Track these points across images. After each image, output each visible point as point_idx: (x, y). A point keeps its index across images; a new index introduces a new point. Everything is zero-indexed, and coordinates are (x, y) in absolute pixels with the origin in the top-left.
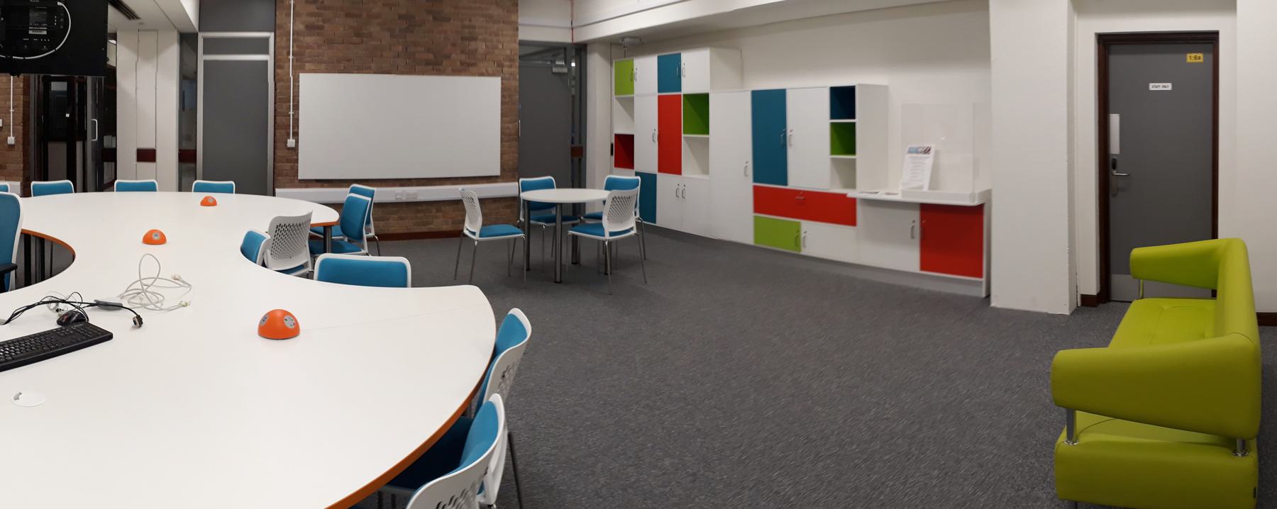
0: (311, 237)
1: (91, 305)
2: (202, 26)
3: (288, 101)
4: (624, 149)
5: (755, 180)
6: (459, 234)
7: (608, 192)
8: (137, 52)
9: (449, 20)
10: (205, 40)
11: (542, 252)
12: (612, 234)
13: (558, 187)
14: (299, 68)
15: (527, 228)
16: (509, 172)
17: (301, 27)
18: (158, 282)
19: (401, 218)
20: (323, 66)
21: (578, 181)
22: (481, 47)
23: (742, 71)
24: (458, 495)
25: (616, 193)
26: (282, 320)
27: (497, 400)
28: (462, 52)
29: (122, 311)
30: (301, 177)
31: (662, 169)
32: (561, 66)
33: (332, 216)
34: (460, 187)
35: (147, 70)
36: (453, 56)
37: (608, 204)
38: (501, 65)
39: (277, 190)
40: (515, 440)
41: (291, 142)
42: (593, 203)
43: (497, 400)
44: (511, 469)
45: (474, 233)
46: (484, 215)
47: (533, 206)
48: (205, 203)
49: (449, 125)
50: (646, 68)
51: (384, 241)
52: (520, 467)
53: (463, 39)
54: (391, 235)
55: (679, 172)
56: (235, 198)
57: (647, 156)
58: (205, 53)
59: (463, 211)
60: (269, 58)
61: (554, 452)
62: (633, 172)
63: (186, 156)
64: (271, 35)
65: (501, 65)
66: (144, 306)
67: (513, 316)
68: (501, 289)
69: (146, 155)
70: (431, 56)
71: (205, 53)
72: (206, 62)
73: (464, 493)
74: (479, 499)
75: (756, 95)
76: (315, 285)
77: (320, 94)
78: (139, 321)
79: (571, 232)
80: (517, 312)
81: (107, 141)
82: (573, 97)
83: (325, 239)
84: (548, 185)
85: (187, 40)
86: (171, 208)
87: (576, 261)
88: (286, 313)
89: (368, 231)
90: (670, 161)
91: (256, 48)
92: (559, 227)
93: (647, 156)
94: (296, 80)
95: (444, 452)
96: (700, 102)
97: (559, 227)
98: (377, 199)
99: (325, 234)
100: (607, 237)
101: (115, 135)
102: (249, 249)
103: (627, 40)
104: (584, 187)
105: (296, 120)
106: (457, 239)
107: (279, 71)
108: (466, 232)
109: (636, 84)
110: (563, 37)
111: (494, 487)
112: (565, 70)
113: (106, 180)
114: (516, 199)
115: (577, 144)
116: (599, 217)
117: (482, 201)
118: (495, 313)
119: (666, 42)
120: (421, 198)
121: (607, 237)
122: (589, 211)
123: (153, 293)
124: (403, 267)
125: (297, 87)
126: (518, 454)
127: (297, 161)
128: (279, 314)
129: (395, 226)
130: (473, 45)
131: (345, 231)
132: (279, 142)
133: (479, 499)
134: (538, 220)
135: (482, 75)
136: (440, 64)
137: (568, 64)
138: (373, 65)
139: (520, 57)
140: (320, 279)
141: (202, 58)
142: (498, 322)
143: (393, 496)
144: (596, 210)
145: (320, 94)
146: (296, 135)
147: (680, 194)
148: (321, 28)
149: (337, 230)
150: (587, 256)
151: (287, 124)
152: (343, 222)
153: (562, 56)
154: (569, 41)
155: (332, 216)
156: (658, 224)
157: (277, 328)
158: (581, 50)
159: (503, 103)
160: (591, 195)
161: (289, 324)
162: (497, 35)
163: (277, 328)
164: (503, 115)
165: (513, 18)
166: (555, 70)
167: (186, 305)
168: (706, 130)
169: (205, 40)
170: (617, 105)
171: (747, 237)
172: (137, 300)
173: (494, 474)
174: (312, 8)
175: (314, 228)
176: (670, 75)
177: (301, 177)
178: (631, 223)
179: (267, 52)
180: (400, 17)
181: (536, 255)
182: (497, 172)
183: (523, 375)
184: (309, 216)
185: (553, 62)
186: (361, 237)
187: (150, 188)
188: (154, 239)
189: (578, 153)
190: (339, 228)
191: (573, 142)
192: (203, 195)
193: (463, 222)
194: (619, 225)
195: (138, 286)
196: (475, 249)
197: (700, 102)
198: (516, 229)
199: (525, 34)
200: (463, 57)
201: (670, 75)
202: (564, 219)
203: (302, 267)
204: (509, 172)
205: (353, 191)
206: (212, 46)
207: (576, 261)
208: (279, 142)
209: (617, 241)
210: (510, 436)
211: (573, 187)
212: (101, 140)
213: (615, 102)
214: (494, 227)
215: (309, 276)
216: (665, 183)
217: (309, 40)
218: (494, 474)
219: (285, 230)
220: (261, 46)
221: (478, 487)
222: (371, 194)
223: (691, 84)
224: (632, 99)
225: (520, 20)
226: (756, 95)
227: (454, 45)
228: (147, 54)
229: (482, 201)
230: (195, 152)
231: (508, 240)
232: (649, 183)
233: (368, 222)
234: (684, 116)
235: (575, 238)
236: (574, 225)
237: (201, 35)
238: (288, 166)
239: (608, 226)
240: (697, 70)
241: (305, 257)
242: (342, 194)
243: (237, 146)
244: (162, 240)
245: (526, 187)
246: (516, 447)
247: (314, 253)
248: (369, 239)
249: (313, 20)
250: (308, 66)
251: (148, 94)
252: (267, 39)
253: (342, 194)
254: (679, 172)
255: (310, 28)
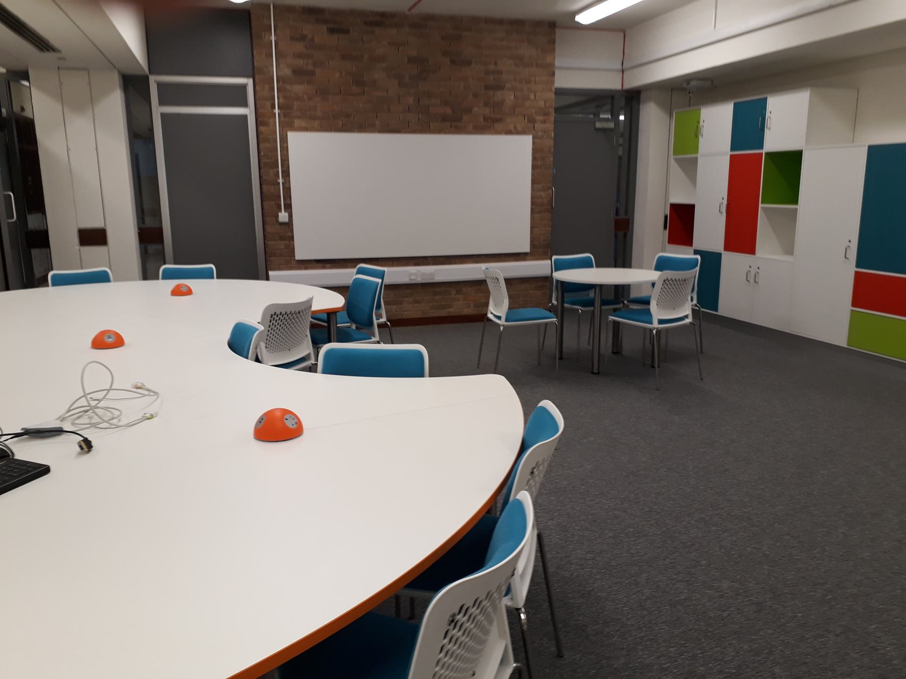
0: (313, 326)
1: (17, 435)
2: (154, 67)
3: (275, 165)
4: (681, 222)
5: (858, 266)
6: (482, 318)
7: (658, 273)
8: (61, 98)
9: (469, 63)
10: (160, 86)
11: (577, 338)
12: (661, 322)
13: (597, 266)
14: (288, 125)
15: (561, 313)
16: (539, 249)
17: (287, 72)
18: (112, 394)
19: (416, 302)
20: (316, 123)
21: (622, 259)
22: (509, 98)
23: (855, 120)
24: (483, 597)
25: (669, 274)
26: (282, 419)
27: (525, 498)
28: (486, 105)
29: (64, 437)
30: (299, 256)
31: (730, 246)
32: (607, 120)
33: (336, 301)
34: (483, 266)
35: (80, 125)
36: (475, 109)
37: (658, 286)
38: (532, 120)
39: (271, 273)
40: (546, 541)
41: (283, 216)
42: (639, 285)
43: (525, 498)
44: (541, 564)
45: (499, 318)
46: (510, 297)
47: (567, 288)
48: (177, 292)
49: (473, 193)
50: (717, 121)
51: (396, 327)
52: (551, 570)
53: (487, 88)
54: (404, 320)
55: (751, 250)
56: (216, 284)
57: (710, 230)
58: (162, 103)
59: (487, 293)
60: (248, 111)
61: (589, 556)
62: (691, 249)
63: (149, 236)
64: (249, 82)
65: (532, 120)
66: (94, 425)
67: (544, 409)
68: (528, 379)
69: (93, 237)
70: (448, 111)
71: (245, 117)
72: (164, 116)
73: (489, 595)
74: (506, 601)
75: (876, 154)
76: (319, 379)
77: (311, 155)
78: (87, 445)
79: (611, 318)
80: (547, 404)
81: (33, 222)
82: (620, 158)
83: (329, 327)
84: (586, 264)
85: (134, 86)
86: (130, 302)
87: (617, 350)
88: (286, 412)
89: (379, 316)
90: (741, 237)
91: (230, 97)
92: (597, 312)
93: (710, 230)
94: (284, 140)
95: (468, 550)
96: (789, 164)
97: (597, 312)
98: (388, 280)
99: (328, 321)
100: (655, 324)
101: (43, 212)
102: (239, 342)
103: (694, 83)
104: (630, 266)
105: (288, 190)
106: (480, 324)
107: (262, 128)
108: (490, 316)
109: (702, 141)
110: (610, 82)
111: (522, 589)
112: (611, 125)
113: (38, 273)
114: (548, 279)
115: (622, 216)
116: (646, 302)
117: (508, 281)
118: (523, 405)
119: (744, 85)
120: (439, 278)
121: (655, 324)
122: (634, 295)
123: (106, 409)
124: (419, 355)
125: (285, 149)
126: (548, 556)
127: (292, 238)
128: (278, 414)
129: (410, 310)
130: (499, 95)
131: (352, 319)
132: (269, 215)
133: (506, 601)
134: (574, 303)
135: (509, 132)
136: (460, 120)
137: (615, 117)
138: (377, 123)
139: (557, 110)
140: (325, 372)
141: (158, 110)
142: (526, 415)
143: (412, 600)
144: (643, 294)
145: (311, 155)
146: (288, 207)
147: (752, 278)
148: (312, 73)
149: (343, 316)
150: (629, 345)
151: (277, 195)
152: (349, 307)
153: (608, 107)
154: (618, 87)
155: (336, 301)
156: (719, 313)
157: (276, 428)
158: (632, 99)
159: (534, 167)
160: (638, 276)
161: (290, 424)
162: (528, 82)
163: (276, 428)
164: (534, 182)
165: (549, 59)
166: (598, 125)
167: (152, 417)
168: (794, 198)
169: (160, 86)
170: (675, 167)
171: (841, 340)
172: (85, 420)
173: (523, 575)
174: (299, 47)
175: (315, 315)
176: (749, 127)
177: (299, 256)
178: (686, 310)
179: (245, 104)
180: (411, 60)
181: (570, 342)
182: (526, 248)
183: (553, 472)
184: (309, 303)
185: (596, 115)
186: (371, 324)
187: (102, 278)
188: (107, 341)
189: (623, 226)
190: (345, 313)
191: (617, 213)
192: (173, 283)
193: (487, 304)
194: (671, 312)
195: (83, 402)
196: (502, 335)
197: (789, 164)
198: (551, 314)
199: (563, 80)
200: (487, 111)
201: (749, 127)
202: (604, 303)
203: (303, 360)
204: (539, 249)
205: (360, 271)
206: (169, 94)
207: (617, 350)
208: (269, 215)
209: (667, 330)
210: (540, 537)
211: (616, 266)
212: (22, 218)
213: (674, 165)
214: (522, 310)
215: (312, 369)
216: (733, 265)
217: (298, 89)
218: (523, 575)
219: (281, 319)
220: (236, 96)
221: (504, 588)
222: (381, 275)
223: (775, 140)
224: (697, 158)
225: (558, 62)
226: (876, 154)
227: (475, 95)
228: (86, 103)
229: (508, 281)
230: (160, 230)
231: (539, 325)
232: (710, 265)
233: (379, 307)
234: (766, 180)
235: (616, 324)
236: (615, 310)
237: (153, 80)
238: (281, 245)
239: (657, 313)
240: (788, 119)
241: (306, 348)
242: (348, 276)
243: (212, 220)
244: (119, 342)
245: (559, 266)
246: (546, 549)
247: (317, 343)
248: (380, 326)
249: (300, 62)
250: (297, 122)
251: (87, 159)
252: (244, 87)
253: (348, 276)
254: (751, 250)
255: (298, 73)
